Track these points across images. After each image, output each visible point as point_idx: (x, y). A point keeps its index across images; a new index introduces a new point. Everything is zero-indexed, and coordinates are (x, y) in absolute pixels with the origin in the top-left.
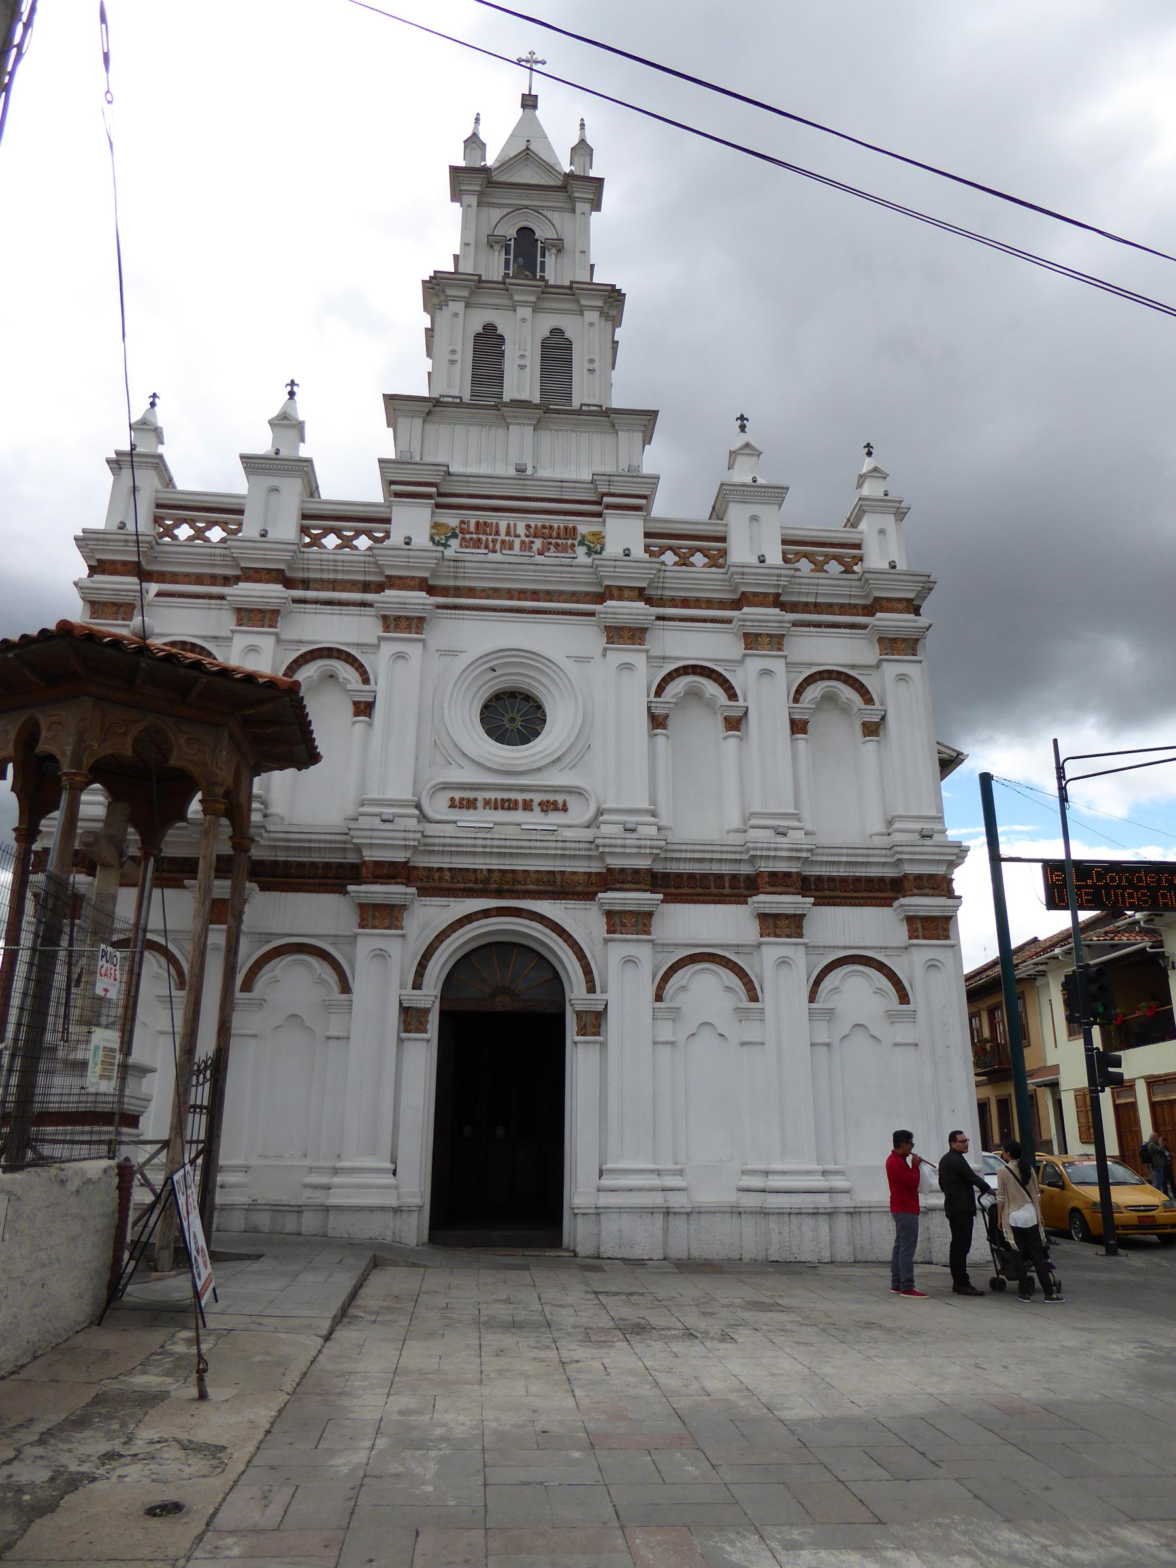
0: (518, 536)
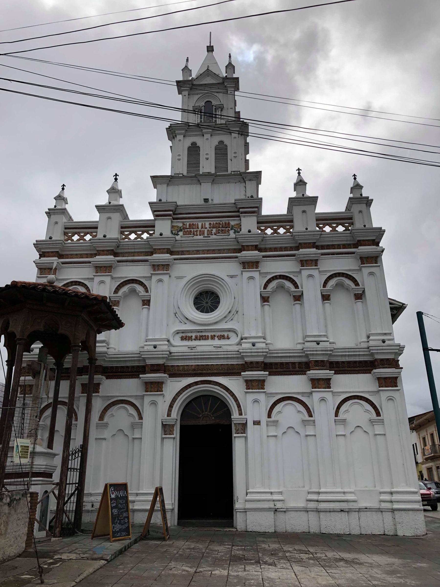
0: (207, 228)
